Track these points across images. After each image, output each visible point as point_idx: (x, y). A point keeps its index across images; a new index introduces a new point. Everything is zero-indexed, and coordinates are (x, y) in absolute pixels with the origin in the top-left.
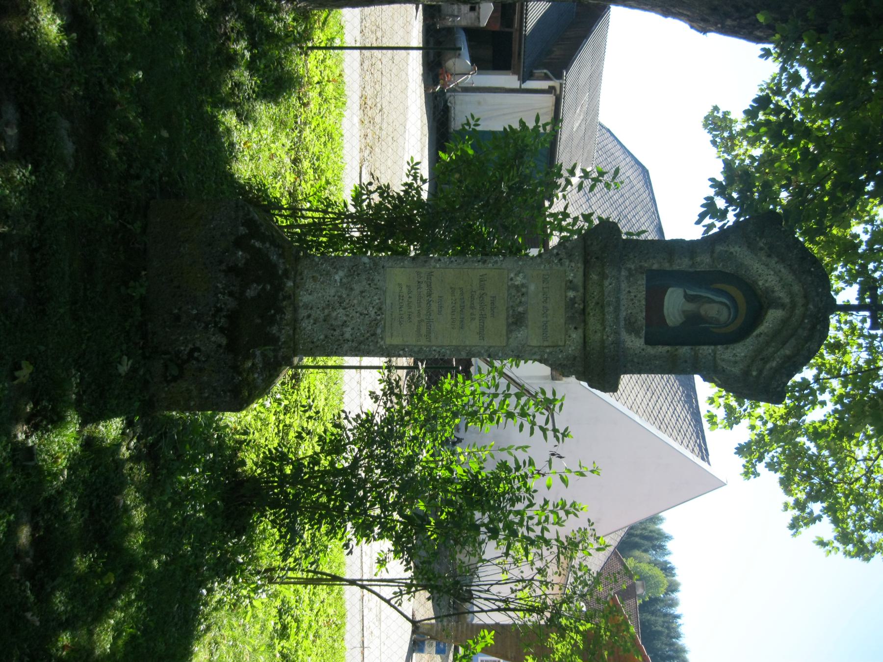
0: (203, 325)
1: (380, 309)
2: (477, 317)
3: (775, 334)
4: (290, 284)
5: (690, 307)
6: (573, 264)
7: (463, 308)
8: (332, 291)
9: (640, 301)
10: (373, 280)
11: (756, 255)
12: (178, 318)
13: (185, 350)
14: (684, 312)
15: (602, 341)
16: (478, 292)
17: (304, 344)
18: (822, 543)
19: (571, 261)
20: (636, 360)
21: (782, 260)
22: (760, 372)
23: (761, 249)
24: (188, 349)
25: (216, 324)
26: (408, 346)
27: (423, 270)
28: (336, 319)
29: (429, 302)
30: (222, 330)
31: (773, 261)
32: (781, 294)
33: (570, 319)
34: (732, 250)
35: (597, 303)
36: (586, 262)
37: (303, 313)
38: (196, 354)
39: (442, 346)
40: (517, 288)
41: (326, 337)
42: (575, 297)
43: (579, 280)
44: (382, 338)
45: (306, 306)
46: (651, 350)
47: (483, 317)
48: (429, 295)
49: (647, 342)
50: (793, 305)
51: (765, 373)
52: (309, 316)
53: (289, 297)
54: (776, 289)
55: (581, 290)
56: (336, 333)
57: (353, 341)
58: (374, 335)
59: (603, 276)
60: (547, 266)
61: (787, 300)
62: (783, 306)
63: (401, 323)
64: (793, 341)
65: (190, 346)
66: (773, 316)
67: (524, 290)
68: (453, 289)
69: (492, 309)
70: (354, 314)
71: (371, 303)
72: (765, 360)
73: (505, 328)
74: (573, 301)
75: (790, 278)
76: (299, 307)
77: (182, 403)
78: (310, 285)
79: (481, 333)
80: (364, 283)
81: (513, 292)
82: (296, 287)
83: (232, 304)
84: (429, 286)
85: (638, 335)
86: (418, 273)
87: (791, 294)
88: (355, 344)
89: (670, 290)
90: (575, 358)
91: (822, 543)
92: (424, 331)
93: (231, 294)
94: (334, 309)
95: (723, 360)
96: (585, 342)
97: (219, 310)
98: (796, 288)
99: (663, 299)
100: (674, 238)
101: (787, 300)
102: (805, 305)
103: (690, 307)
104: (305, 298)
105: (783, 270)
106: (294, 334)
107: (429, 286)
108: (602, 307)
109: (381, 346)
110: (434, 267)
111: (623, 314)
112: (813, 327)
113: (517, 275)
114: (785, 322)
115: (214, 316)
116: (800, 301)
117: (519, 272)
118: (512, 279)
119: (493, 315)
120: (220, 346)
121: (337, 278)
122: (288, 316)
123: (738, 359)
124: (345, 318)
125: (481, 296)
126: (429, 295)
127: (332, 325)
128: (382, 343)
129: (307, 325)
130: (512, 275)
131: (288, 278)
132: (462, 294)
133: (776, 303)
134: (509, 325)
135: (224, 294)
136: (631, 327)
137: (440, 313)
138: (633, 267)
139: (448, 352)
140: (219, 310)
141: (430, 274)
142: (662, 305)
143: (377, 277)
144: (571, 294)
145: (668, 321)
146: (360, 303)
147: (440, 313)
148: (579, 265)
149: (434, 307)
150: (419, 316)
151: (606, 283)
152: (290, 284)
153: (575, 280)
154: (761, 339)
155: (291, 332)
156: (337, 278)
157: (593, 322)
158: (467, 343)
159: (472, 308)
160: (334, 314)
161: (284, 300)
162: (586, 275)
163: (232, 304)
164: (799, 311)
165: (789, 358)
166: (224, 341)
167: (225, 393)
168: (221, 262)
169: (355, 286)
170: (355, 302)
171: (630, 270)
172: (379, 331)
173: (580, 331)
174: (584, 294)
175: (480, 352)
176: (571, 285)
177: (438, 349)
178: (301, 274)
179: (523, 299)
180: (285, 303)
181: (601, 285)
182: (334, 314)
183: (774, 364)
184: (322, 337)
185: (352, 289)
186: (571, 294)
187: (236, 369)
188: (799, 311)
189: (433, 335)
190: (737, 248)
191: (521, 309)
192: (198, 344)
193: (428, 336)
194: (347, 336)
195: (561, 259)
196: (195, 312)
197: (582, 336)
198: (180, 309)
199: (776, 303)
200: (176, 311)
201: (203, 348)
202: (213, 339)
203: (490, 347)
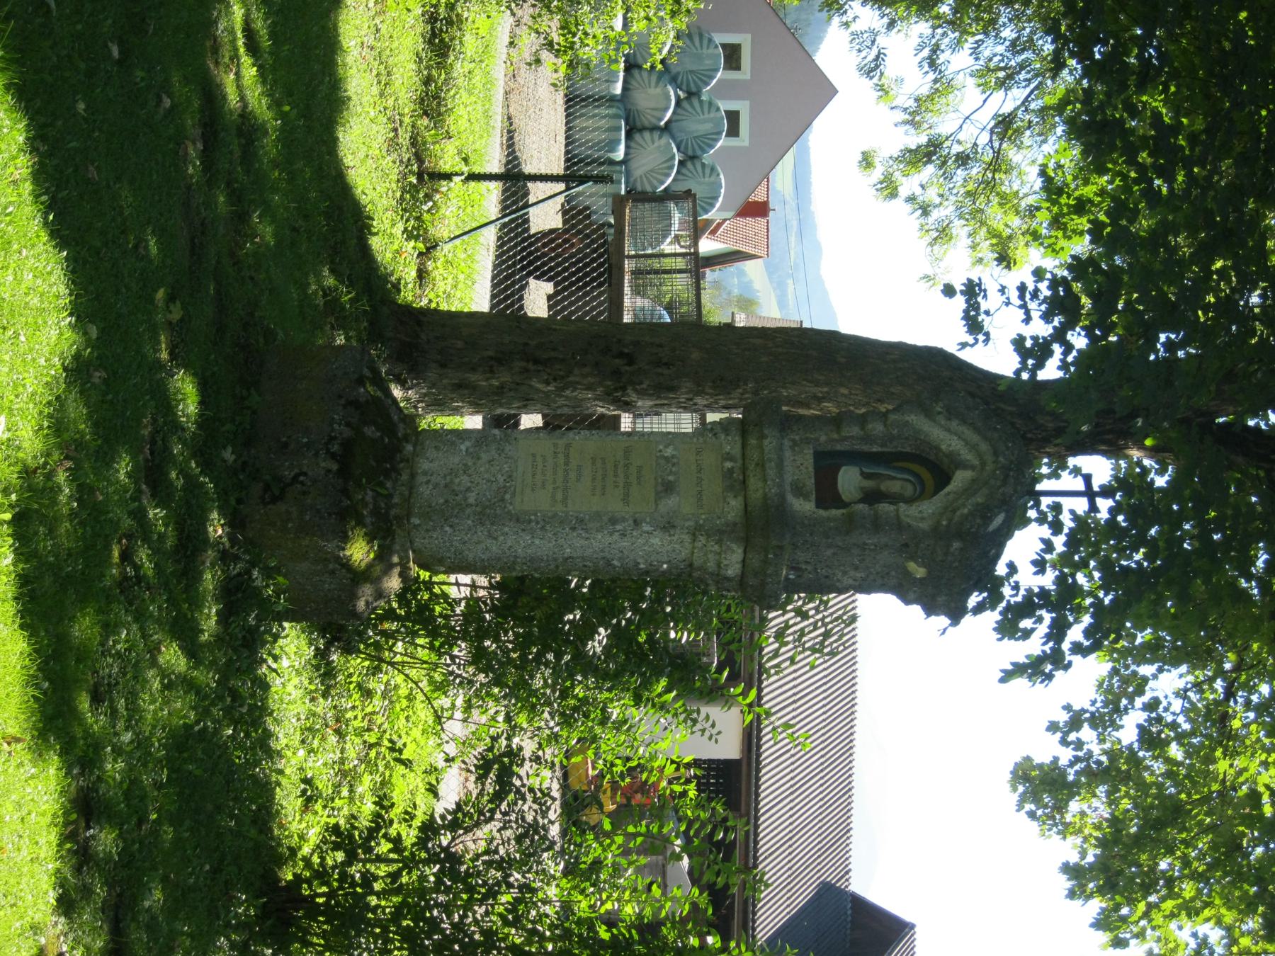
0: (313, 452)
1: (510, 477)
2: (621, 485)
4: (409, 448)
5: (869, 484)
6: (730, 438)
7: (604, 476)
8: (457, 460)
9: (807, 468)
10: (503, 450)
11: (934, 421)
12: (286, 445)
13: (288, 474)
14: (862, 489)
16: (622, 463)
17: (420, 507)
19: (727, 435)
20: (806, 522)
21: (964, 421)
22: (950, 520)
23: (939, 413)
24: (293, 474)
25: (328, 451)
26: (540, 511)
27: (561, 442)
28: (459, 484)
29: (566, 471)
30: (333, 456)
31: (954, 424)
32: (967, 455)
33: (730, 488)
34: (907, 418)
35: (757, 465)
37: (421, 479)
38: (302, 478)
39: (580, 512)
40: (667, 459)
41: (446, 501)
42: (733, 468)
43: (737, 451)
44: (511, 504)
45: (425, 473)
47: (627, 485)
48: (566, 464)
49: (818, 506)
50: (983, 464)
52: (428, 482)
53: (408, 461)
54: (962, 452)
55: (740, 462)
56: (458, 498)
57: (477, 506)
58: (503, 500)
60: (701, 440)
61: (976, 462)
62: (973, 468)
63: (533, 490)
65: (296, 471)
67: (675, 460)
68: (594, 460)
69: (638, 478)
70: (480, 480)
71: (500, 470)
73: (653, 494)
74: (731, 471)
75: (975, 438)
76: (417, 473)
77: (279, 524)
79: (626, 499)
80: (493, 452)
81: (662, 462)
82: (415, 454)
83: (347, 432)
84: (567, 456)
85: (806, 497)
86: (555, 445)
87: (980, 456)
88: (479, 509)
89: (843, 468)
90: (735, 524)
92: (559, 496)
93: (348, 424)
94: (456, 476)
95: (908, 516)
96: (746, 506)
97: (332, 439)
98: (984, 447)
99: (837, 474)
100: (811, 150)
101: (976, 462)
103: (869, 484)
104: (424, 465)
105: (966, 431)
106: (410, 497)
107: (567, 456)
108: (763, 466)
109: (509, 512)
110: (574, 439)
113: (666, 447)
115: (326, 444)
116: (989, 458)
117: (669, 445)
118: (660, 451)
119: (639, 483)
120: (329, 471)
121: (463, 447)
122: (405, 477)
123: (925, 515)
124: (469, 484)
125: (626, 466)
126: (566, 464)
127: (453, 491)
128: (511, 508)
129: (425, 491)
130: (661, 447)
131: (407, 442)
132: (604, 463)
133: (963, 465)
134: (657, 493)
135: (340, 425)
136: (799, 491)
137: (578, 480)
138: (797, 438)
139: (587, 517)
140: (332, 439)
141: (568, 446)
142: (836, 483)
143: (508, 448)
144: (728, 465)
145: (843, 497)
146: (487, 471)
147: (578, 480)
148: (737, 438)
149: (572, 475)
150: (554, 482)
151: (766, 442)
152: (409, 448)
153: (733, 452)
154: (951, 497)
155: (407, 493)
156: (463, 447)
157: (754, 483)
158: (610, 509)
159: (616, 476)
160: (457, 481)
161: (402, 462)
162: (744, 446)
163: (347, 432)
164: (989, 467)
166: (335, 467)
167: (330, 514)
169: (482, 455)
170: (482, 469)
171: (793, 441)
172: (507, 496)
173: (740, 499)
174: (744, 464)
175: (624, 518)
176: (729, 457)
177: (576, 514)
178: (422, 444)
179: (674, 469)
180: (402, 465)
181: (761, 447)
182: (457, 481)
183: (966, 511)
184: (441, 501)
185: (479, 458)
186: (728, 465)
187: (345, 492)
189: (570, 502)
190: (913, 417)
191: (671, 478)
192: (305, 469)
193: (565, 501)
194: (471, 500)
195: (715, 434)
196: (305, 440)
197: (743, 503)
198: (289, 437)
199: (963, 465)
200: (284, 439)
201: (310, 473)
202: (323, 464)
203: (636, 513)
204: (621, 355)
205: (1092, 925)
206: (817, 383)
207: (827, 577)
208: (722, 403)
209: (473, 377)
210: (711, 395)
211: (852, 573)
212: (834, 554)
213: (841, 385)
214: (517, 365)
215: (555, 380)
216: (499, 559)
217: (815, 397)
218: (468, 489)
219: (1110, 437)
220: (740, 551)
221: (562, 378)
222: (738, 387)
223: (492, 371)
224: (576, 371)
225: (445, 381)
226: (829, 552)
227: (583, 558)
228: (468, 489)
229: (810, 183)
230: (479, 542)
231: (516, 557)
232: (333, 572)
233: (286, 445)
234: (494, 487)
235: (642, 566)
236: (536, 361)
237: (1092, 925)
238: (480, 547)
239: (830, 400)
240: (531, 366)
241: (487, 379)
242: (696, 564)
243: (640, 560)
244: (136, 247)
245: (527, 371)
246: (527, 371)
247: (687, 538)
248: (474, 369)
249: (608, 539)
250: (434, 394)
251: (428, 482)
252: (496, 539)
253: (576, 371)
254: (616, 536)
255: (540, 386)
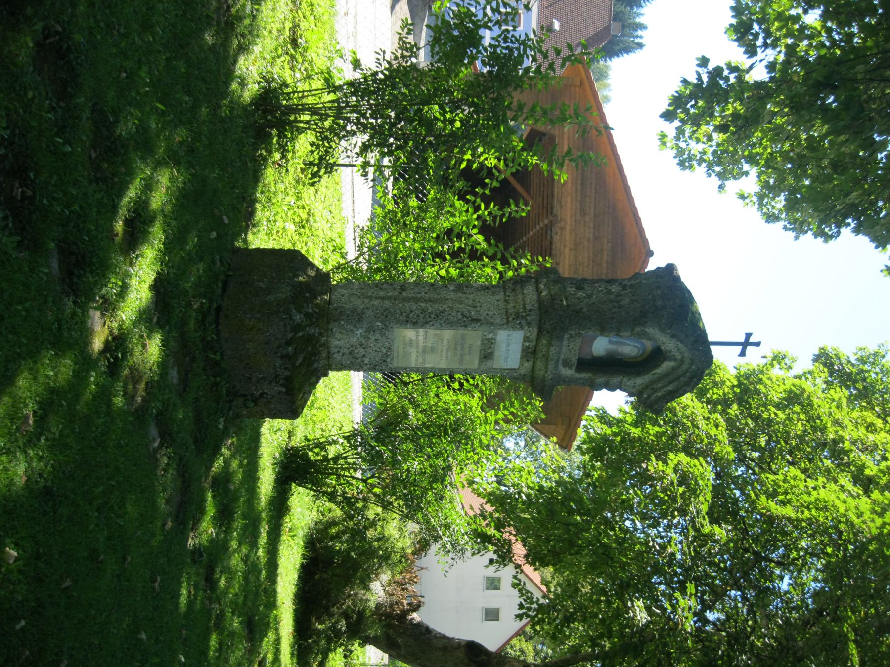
3: (666, 375)
8: (355, 340)
12: (250, 379)
15: (544, 377)
18: (742, 197)
22: (649, 396)
36: (540, 331)
40: (489, 340)
45: (336, 347)
46: (578, 375)
47: (462, 356)
51: (652, 398)
55: (534, 343)
59: (550, 345)
62: (676, 360)
64: (676, 383)
65: (260, 392)
66: (666, 366)
72: (655, 391)
74: (528, 348)
78: (338, 336)
85: (570, 367)
91: (742, 197)
94: (356, 348)
102: (691, 364)
104: (334, 342)
111: (562, 357)
112: (691, 379)
114: (674, 369)
116: (687, 361)
122: (324, 355)
143: (387, 333)
151: (552, 349)
154: (656, 376)
164: (684, 367)
165: (671, 392)
166: (284, 390)
168: (277, 353)
171: (571, 335)
172: (389, 360)
173: (531, 363)
182: (356, 351)
183: (659, 394)
185: (369, 339)
188: (684, 367)
205: (662, 116)
218: (364, 356)
228: (364, 356)
229: (608, 128)
233: (250, 379)
234: (380, 354)
237: (662, 116)
251: (339, 352)
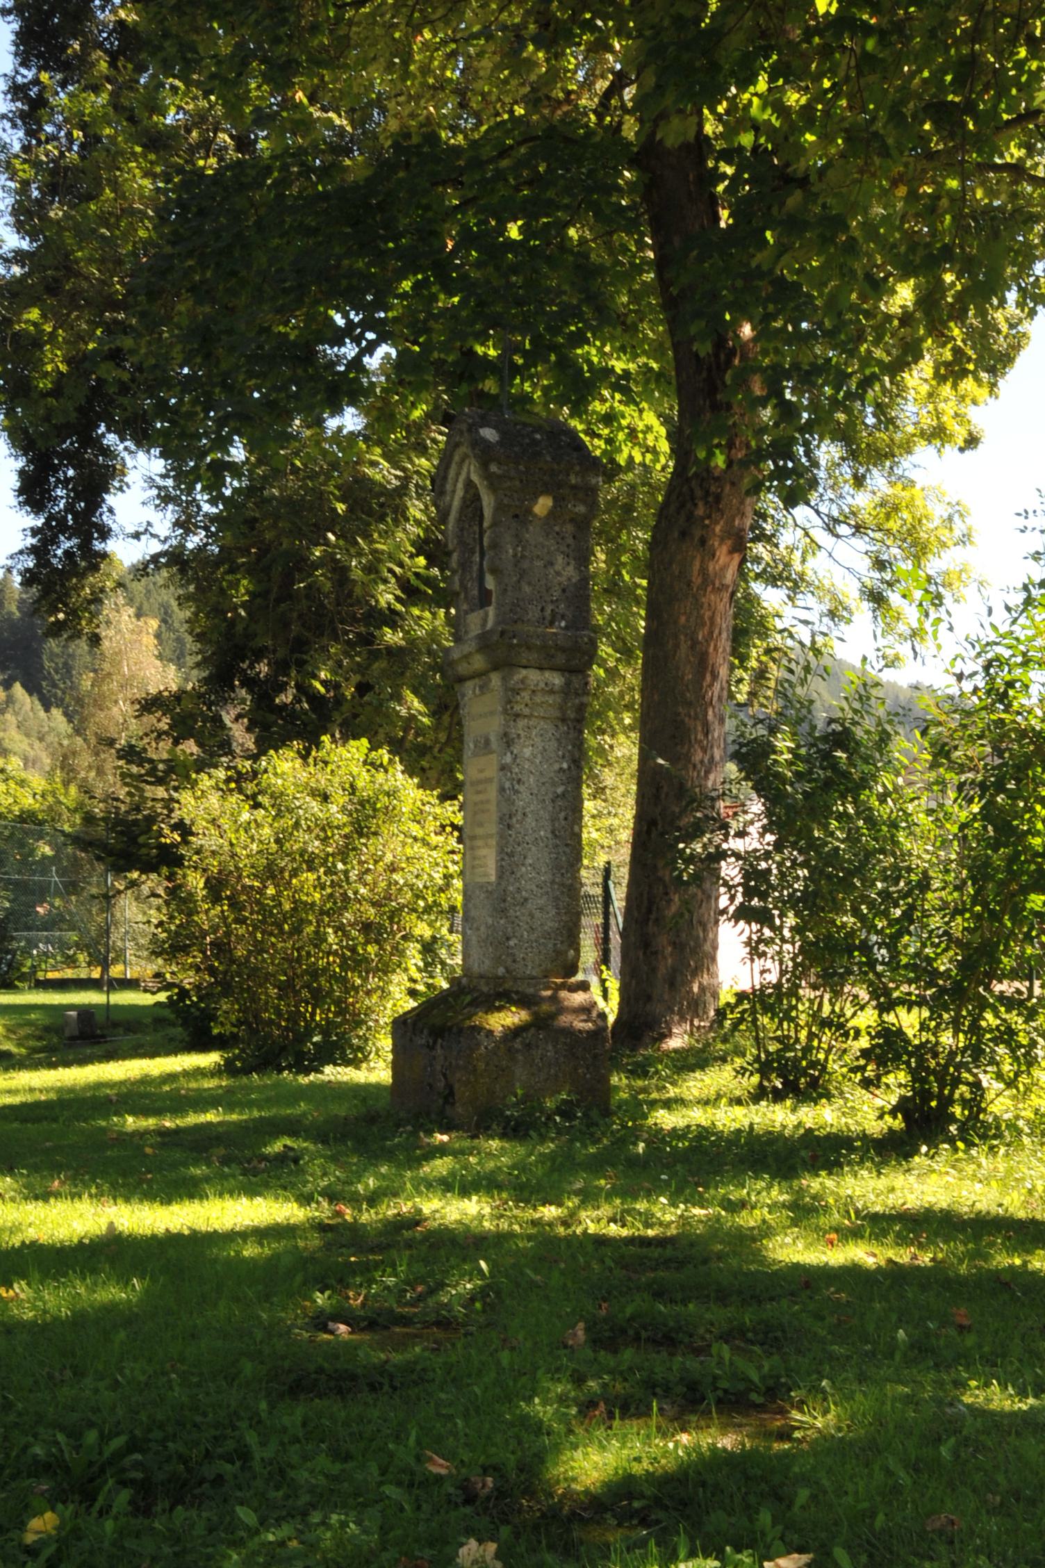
204: (648, 832)
206: (677, 646)
207: (564, 591)
208: (700, 736)
209: (662, 971)
210: (691, 745)
211: (558, 567)
212: (529, 584)
213: (676, 622)
214: (651, 928)
215: (667, 894)
216: (557, 899)
217: (692, 647)
219: (722, 357)
220: (524, 672)
221: (665, 887)
222: (683, 722)
223: (656, 953)
224: (660, 874)
225: (666, 997)
226: (527, 589)
227: (553, 820)
230: (532, 916)
231: (553, 882)
232: (528, 1046)
235: (565, 766)
236: (649, 911)
238: (537, 914)
239: (695, 632)
240: (653, 916)
241: (665, 958)
242: (558, 714)
243: (557, 767)
244: (831, 1357)
245: (657, 920)
246: (657, 920)
247: (522, 723)
248: (654, 970)
249: (525, 795)
250: (680, 1009)
252: (526, 900)
253: (660, 874)
254: (521, 788)
255: (674, 909)
